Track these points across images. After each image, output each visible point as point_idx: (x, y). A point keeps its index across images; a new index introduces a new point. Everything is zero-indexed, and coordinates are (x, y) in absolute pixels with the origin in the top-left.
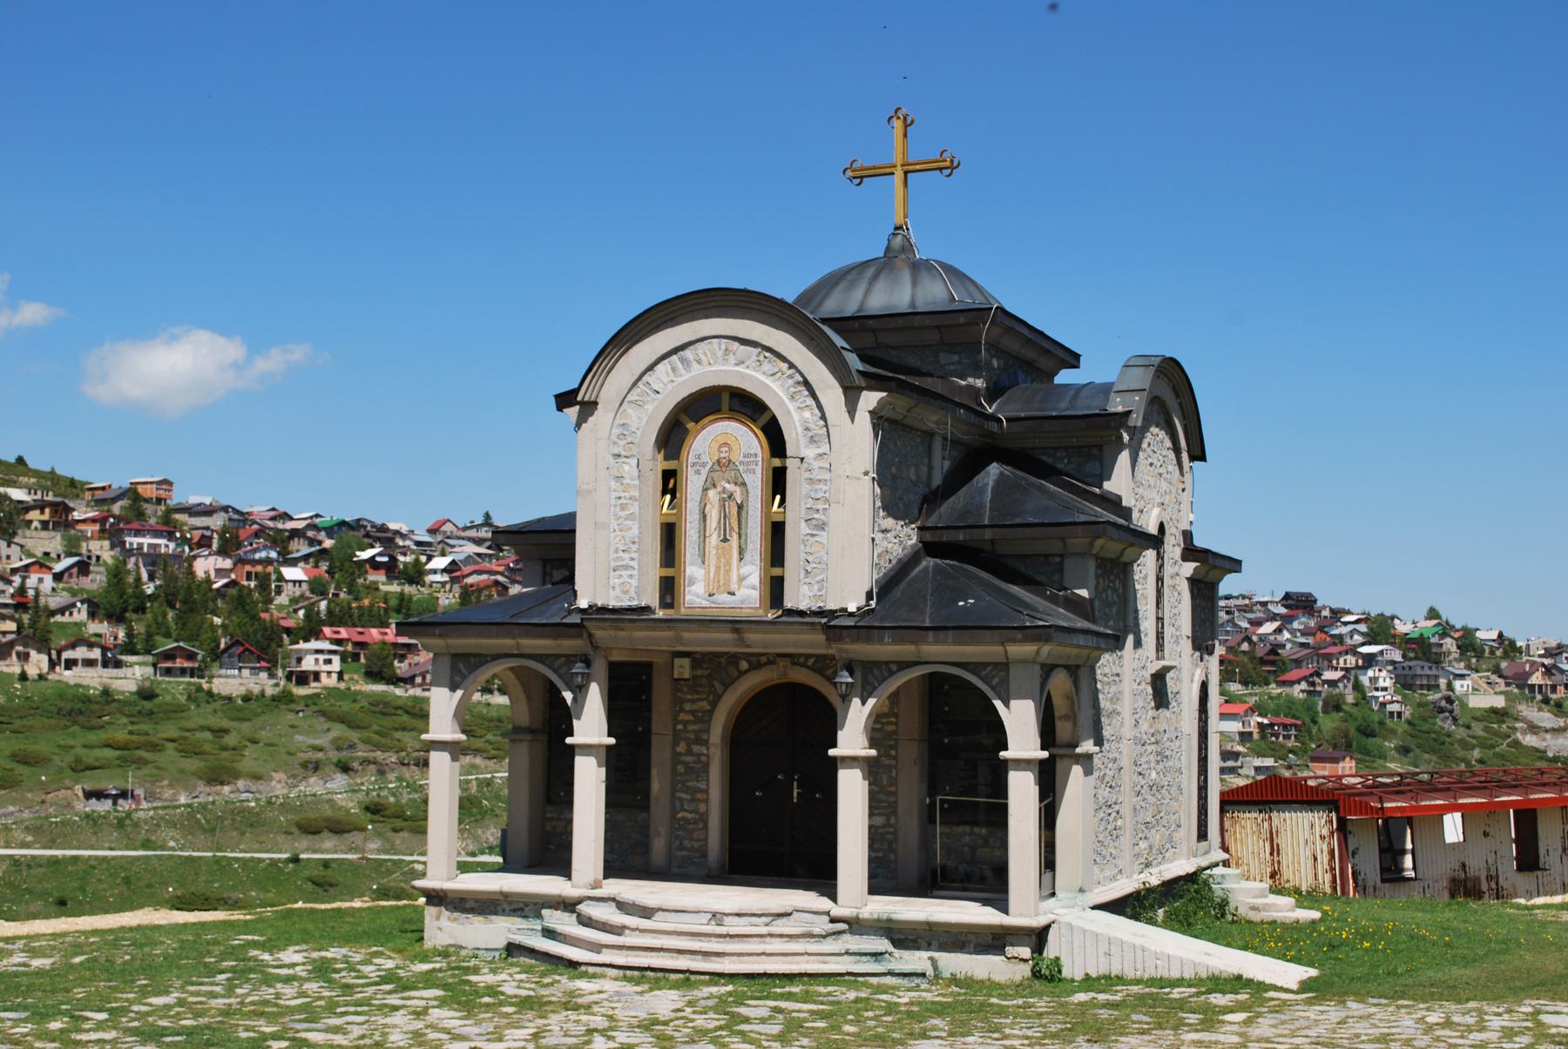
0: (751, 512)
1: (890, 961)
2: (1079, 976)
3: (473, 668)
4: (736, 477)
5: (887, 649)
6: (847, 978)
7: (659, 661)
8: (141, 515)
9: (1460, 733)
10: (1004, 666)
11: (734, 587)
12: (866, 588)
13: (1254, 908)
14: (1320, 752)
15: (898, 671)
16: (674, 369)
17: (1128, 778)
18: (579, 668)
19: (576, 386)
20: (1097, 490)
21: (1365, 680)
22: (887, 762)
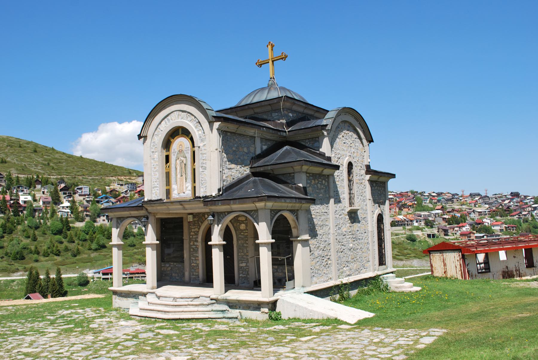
0: (188, 166)
1: (228, 313)
3: (121, 222)
4: (184, 155)
6: (209, 319)
7: (184, 216)
10: (256, 211)
11: (185, 191)
12: (218, 187)
13: (397, 287)
14: (522, 233)
15: (228, 214)
16: (166, 123)
17: (334, 248)
19: (139, 133)
20: (318, 152)
21: (534, 214)
22: (246, 245)
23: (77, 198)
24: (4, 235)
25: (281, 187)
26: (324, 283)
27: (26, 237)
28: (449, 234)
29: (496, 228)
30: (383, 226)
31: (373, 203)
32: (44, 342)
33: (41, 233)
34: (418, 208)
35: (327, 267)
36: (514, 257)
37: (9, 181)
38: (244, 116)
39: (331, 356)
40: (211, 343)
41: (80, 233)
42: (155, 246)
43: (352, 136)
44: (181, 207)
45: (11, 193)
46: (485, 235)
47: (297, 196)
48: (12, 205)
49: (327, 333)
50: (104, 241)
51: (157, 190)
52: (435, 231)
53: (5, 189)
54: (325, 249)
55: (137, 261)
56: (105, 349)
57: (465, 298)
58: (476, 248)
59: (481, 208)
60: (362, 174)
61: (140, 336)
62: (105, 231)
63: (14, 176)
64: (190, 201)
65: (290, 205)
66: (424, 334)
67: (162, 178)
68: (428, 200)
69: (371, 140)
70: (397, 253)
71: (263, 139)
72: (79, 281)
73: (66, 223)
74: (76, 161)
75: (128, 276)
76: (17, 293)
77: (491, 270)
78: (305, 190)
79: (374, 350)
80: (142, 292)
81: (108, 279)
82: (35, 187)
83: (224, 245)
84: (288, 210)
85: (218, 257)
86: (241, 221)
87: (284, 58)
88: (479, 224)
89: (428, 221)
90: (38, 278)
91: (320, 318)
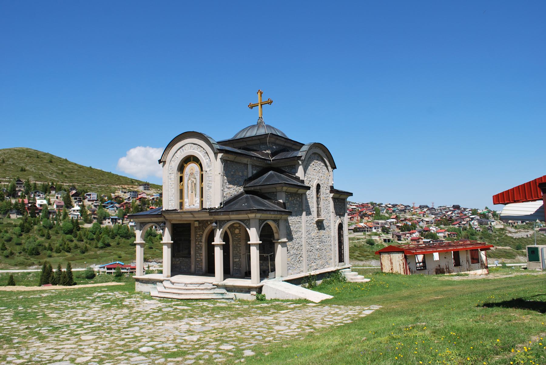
3: (144, 226)
7: (192, 223)
9: (494, 234)
10: (249, 220)
11: (194, 204)
12: (220, 202)
13: (352, 279)
16: (181, 152)
17: (305, 248)
19: (160, 159)
20: (295, 176)
21: (471, 223)
23: (86, 202)
25: (266, 202)
26: (297, 275)
27: (41, 236)
28: (402, 239)
29: (441, 235)
30: (343, 233)
31: (335, 215)
32: (93, 314)
33: (54, 232)
34: (377, 217)
35: (299, 263)
36: (445, 258)
37: (28, 187)
38: (238, 147)
39: (301, 321)
40: (217, 314)
41: (88, 233)
42: (170, 245)
43: (320, 164)
44: (191, 215)
45: (29, 197)
46: (431, 241)
47: (278, 210)
48: (30, 208)
49: (299, 309)
50: (108, 240)
51: (173, 202)
52: (390, 236)
53: (24, 194)
54: (298, 249)
56: (141, 318)
57: (401, 287)
58: (416, 251)
60: (327, 193)
61: (163, 310)
62: (110, 232)
63: (32, 183)
64: (199, 211)
65: (273, 216)
66: (367, 308)
67: (177, 193)
68: (385, 210)
69: (334, 167)
70: (359, 255)
71: (254, 165)
72: (87, 274)
73: (76, 224)
74: (86, 171)
77: (427, 268)
78: (284, 205)
79: (331, 318)
80: (159, 280)
81: (111, 273)
82: (50, 193)
83: (223, 245)
84: (271, 220)
85: (218, 254)
86: (236, 227)
87: (270, 103)
88: (427, 231)
89: (384, 228)
90: (51, 271)
91: (294, 299)
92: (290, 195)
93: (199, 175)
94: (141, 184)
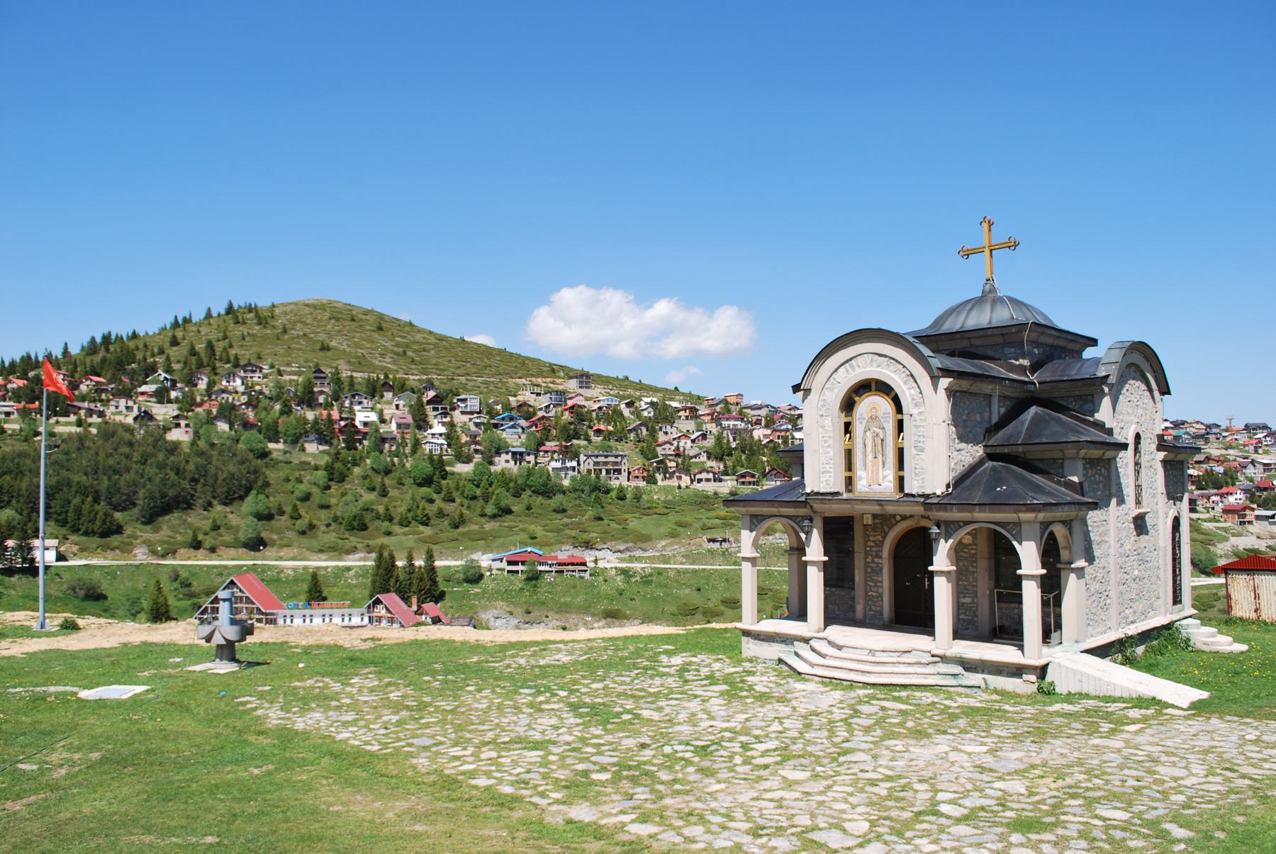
2: (1065, 692)
3: (760, 522)
5: (955, 515)
8: (729, 411)
10: (1018, 524)
11: (881, 482)
12: (946, 482)
13: (1205, 644)
17: (1113, 578)
18: (806, 523)
20: (1091, 419)
23: (458, 417)
24: (332, 483)
27: (368, 489)
28: (1199, 508)
33: (395, 482)
55: (571, 541)
59: (1269, 457)
62: (511, 481)
73: (439, 465)
75: (553, 569)
76: (357, 591)
81: (517, 572)
82: (382, 396)
88: (1265, 489)
90: (394, 565)
92: (1091, 463)
93: (891, 421)
94: (571, 374)
